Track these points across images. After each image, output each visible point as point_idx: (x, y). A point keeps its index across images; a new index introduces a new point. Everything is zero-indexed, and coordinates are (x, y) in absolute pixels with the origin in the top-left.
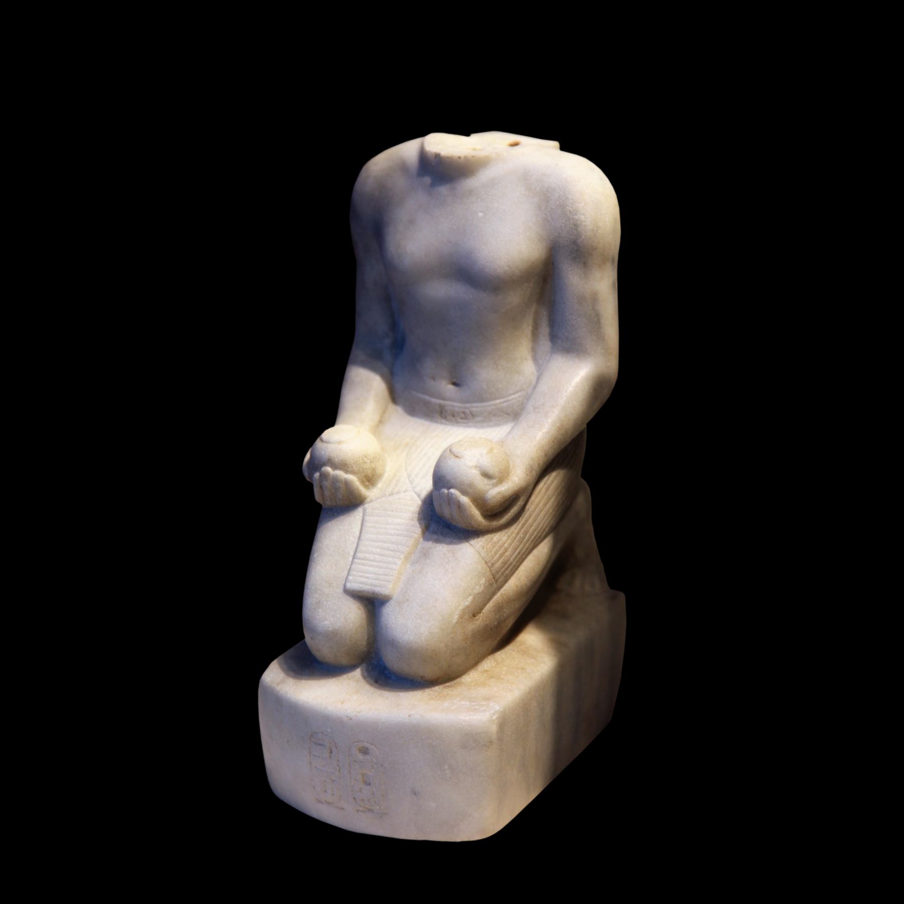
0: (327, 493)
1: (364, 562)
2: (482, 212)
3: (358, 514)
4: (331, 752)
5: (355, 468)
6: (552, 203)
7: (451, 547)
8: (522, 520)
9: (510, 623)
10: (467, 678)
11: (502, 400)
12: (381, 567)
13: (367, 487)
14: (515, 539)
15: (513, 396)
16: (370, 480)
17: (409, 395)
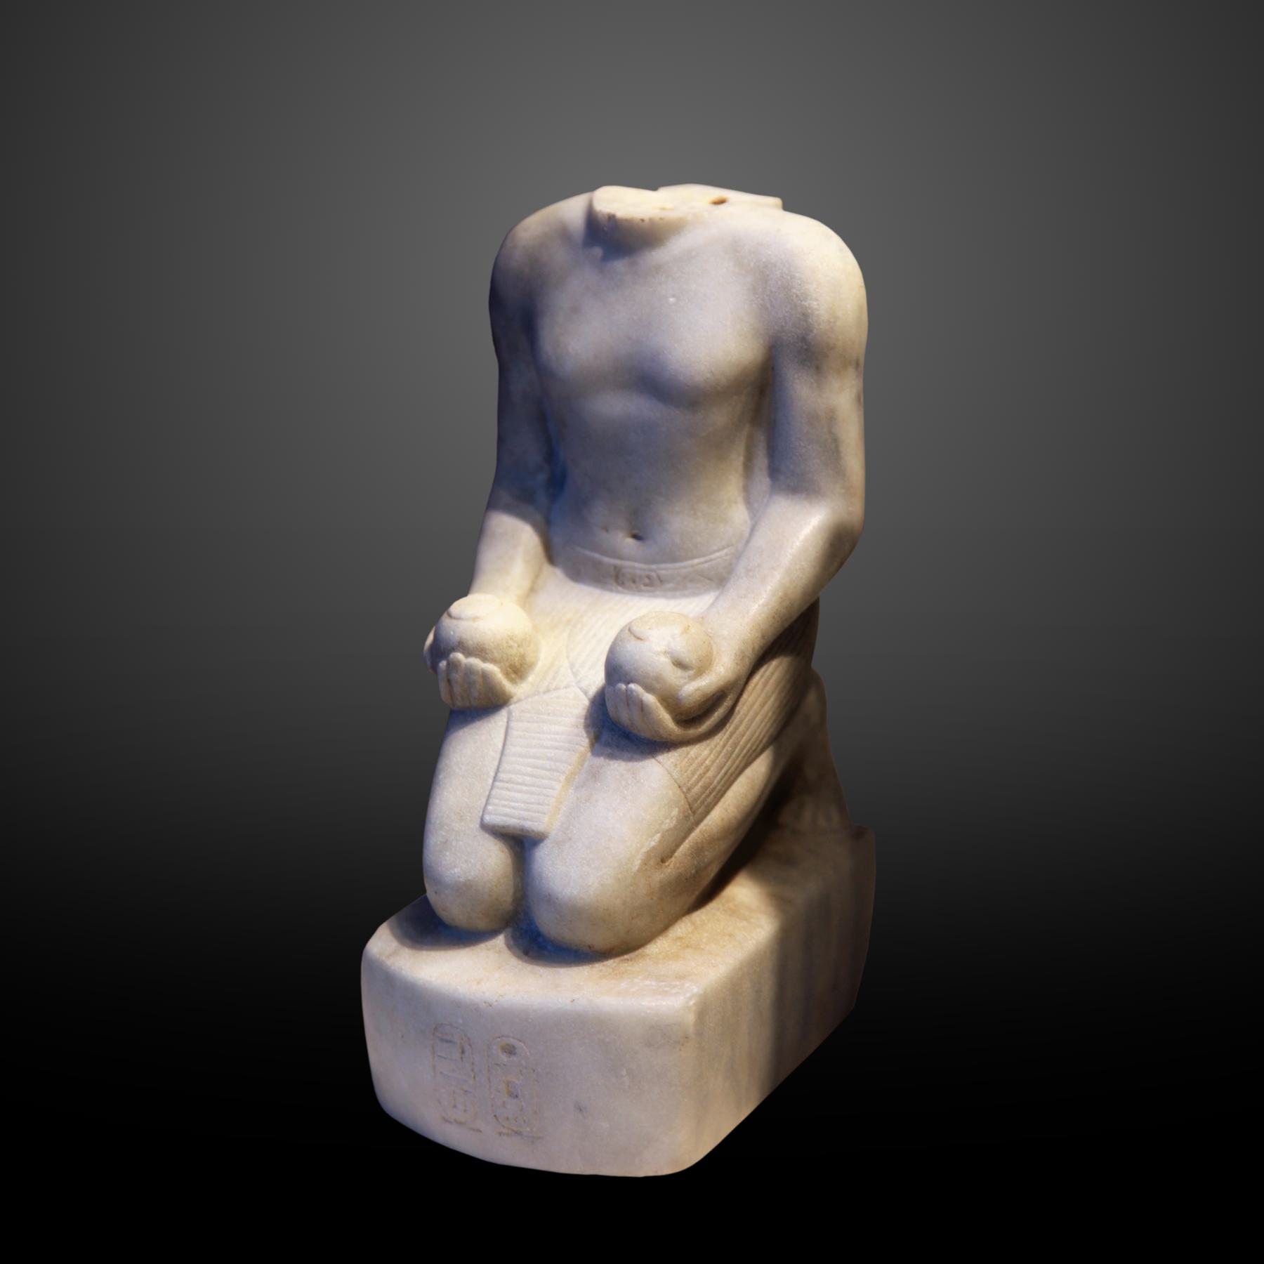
0: (457, 689)
1: (509, 786)
2: (673, 296)
3: (500, 719)
4: (463, 1052)
5: (497, 655)
6: (772, 285)
7: (630, 765)
8: (730, 728)
9: (713, 871)
10: (653, 949)
11: (702, 560)
12: (532, 793)
13: (513, 681)
14: (720, 753)
15: (718, 554)
16: (517, 671)
17: (572, 552)
